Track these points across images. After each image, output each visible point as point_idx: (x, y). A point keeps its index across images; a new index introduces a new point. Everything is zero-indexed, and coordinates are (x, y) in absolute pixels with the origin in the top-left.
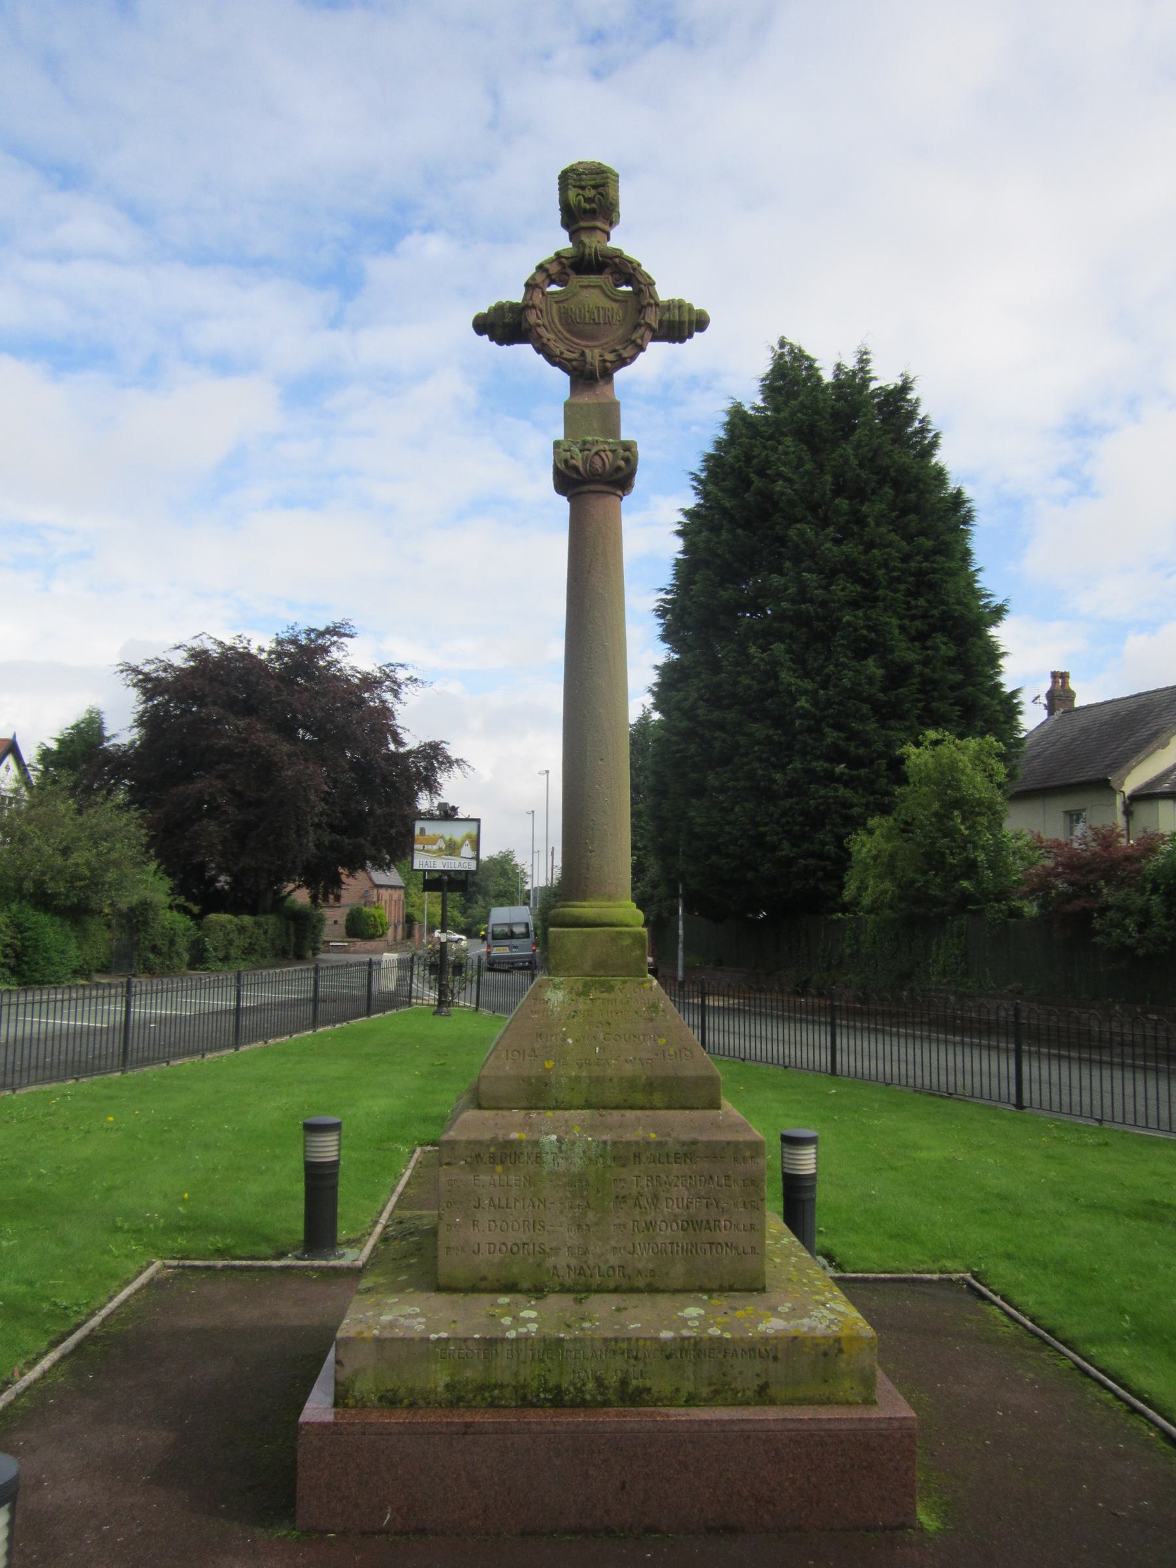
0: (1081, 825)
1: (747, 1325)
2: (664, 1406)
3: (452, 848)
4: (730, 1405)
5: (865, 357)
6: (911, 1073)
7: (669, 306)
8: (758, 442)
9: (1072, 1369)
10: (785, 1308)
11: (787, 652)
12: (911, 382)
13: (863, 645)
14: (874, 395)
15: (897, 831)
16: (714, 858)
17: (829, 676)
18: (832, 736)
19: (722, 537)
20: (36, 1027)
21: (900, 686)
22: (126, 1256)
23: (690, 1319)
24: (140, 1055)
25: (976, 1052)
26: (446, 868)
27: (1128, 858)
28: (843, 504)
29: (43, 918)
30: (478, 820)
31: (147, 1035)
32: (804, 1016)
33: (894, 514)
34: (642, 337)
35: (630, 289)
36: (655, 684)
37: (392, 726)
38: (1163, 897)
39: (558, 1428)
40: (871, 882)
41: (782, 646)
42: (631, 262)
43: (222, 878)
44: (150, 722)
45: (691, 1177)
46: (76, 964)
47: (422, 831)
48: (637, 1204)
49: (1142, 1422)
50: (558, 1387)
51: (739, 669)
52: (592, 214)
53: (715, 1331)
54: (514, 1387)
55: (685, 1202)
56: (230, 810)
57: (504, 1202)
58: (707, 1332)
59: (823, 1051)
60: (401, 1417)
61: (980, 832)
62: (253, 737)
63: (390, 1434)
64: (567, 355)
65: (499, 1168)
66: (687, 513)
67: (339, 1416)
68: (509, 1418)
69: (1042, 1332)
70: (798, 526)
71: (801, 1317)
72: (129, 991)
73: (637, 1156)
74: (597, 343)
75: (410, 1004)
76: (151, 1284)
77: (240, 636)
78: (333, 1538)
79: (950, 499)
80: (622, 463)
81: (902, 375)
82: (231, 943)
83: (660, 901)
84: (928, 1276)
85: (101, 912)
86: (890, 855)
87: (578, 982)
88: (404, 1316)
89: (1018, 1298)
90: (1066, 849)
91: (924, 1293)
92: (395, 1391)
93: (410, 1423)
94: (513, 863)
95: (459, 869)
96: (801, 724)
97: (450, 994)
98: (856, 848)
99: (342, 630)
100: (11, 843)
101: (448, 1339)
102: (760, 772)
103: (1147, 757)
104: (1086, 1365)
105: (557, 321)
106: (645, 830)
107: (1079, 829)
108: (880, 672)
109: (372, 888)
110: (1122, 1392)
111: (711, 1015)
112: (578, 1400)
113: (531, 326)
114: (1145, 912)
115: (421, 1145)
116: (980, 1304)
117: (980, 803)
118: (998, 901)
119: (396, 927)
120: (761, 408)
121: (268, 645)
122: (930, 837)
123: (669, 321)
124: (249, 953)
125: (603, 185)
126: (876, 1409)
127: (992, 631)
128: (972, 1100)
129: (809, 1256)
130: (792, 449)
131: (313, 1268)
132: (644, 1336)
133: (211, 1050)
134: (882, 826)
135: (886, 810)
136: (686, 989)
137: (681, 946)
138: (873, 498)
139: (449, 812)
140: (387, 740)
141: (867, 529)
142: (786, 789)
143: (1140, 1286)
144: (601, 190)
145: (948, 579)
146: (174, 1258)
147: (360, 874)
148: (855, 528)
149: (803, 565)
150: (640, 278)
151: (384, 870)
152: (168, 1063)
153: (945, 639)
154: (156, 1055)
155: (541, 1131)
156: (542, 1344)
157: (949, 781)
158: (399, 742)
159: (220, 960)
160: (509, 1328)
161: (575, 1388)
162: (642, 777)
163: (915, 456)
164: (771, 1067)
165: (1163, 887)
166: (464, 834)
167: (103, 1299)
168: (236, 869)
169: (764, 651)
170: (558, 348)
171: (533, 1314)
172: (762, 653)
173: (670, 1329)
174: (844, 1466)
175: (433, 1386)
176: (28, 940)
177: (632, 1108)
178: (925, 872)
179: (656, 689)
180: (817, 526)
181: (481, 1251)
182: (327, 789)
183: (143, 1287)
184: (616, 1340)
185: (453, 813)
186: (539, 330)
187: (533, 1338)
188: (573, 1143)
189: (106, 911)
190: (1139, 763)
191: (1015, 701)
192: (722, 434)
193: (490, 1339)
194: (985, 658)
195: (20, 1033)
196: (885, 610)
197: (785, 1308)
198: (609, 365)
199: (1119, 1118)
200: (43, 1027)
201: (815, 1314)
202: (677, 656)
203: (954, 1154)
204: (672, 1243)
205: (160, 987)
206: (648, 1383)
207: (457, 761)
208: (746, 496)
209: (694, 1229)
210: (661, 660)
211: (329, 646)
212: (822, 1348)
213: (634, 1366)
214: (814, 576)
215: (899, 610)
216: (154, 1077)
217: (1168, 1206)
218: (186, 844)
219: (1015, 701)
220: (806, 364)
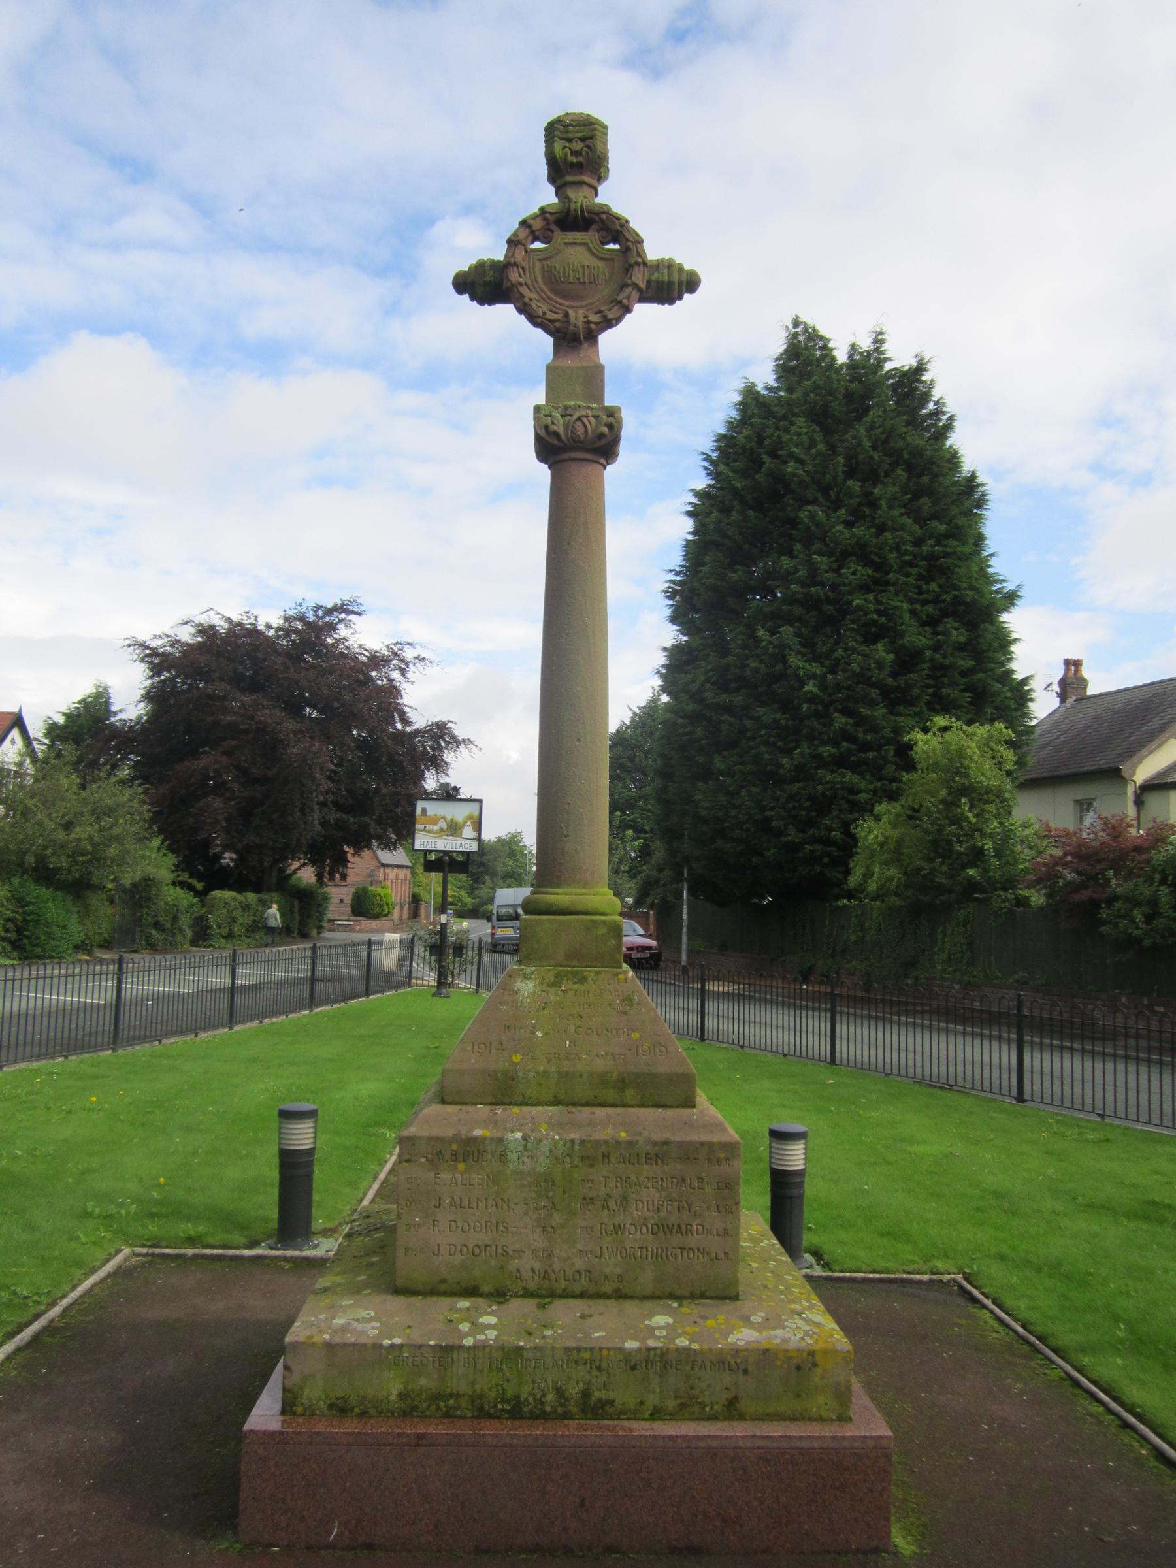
0: (1092, 814)
1: (717, 1336)
2: (628, 1419)
3: (454, 829)
4: (698, 1419)
5: (880, 337)
6: (911, 1063)
7: (658, 265)
9: (1062, 1379)
10: (757, 1318)
11: (797, 635)
12: (926, 363)
13: (873, 629)
14: (889, 375)
16: (719, 843)
17: (838, 660)
18: (840, 721)
19: (733, 518)
20: (32, 1002)
22: (94, 1243)
24: (131, 1033)
25: (977, 1042)
26: (447, 849)
27: (1137, 849)
28: (855, 485)
29: (45, 892)
30: (480, 801)
32: (810, 1004)
34: (628, 298)
35: (617, 247)
36: (663, 666)
37: (399, 704)
38: (1172, 889)
40: (877, 869)
41: (791, 629)
42: (618, 219)
44: (154, 696)
45: (662, 1179)
46: (78, 939)
47: (424, 810)
48: (605, 1206)
49: (1134, 1438)
50: (517, 1397)
52: (579, 167)
53: (682, 1342)
54: (471, 1396)
56: (236, 787)
58: (674, 1343)
60: (350, 1426)
63: (338, 1444)
64: (550, 316)
65: (461, 1166)
66: (697, 494)
67: (285, 1425)
68: (464, 1430)
69: (1032, 1339)
70: (809, 508)
71: (774, 1328)
72: (120, 969)
73: (606, 1156)
74: (583, 303)
75: (409, 985)
76: (117, 1273)
77: (248, 613)
78: (277, 1552)
80: (605, 430)
81: (916, 356)
82: (234, 920)
83: (665, 885)
84: (918, 1277)
85: (104, 887)
86: (897, 842)
87: (549, 972)
88: (357, 1320)
89: (1009, 1303)
90: (1075, 839)
93: (359, 1433)
95: (461, 849)
96: (808, 708)
98: (863, 834)
99: (350, 608)
100: (13, 817)
101: (402, 1346)
102: (767, 756)
103: (1159, 746)
104: (1077, 1375)
105: (539, 279)
107: (1090, 819)
109: (379, 867)
110: (1114, 1405)
111: (711, 1000)
112: (538, 1411)
113: (512, 285)
114: (1153, 903)
116: (973, 1309)
117: (988, 790)
118: (1005, 890)
119: (402, 906)
121: (276, 621)
122: (937, 824)
123: (658, 282)
124: (253, 931)
125: (591, 138)
127: (1004, 617)
128: (973, 1092)
129: (789, 1260)
131: (285, 1259)
132: (609, 1345)
133: (205, 1029)
135: (892, 796)
137: (685, 930)
138: (886, 481)
139: (451, 792)
141: (879, 512)
142: (793, 773)
143: (1136, 1291)
144: (588, 142)
146: (144, 1246)
147: (366, 853)
148: (867, 511)
149: (814, 548)
151: (390, 849)
152: (160, 1042)
153: (956, 625)
154: (148, 1034)
155: (505, 1129)
156: (500, 1353)
157: (957, 768)
158: (406, 721)
159: (224, 937)
160: (466, 1335)
162: (650, 760)
163: (929, 439)
164: (770, 1054)
165: (1170, 878)
167: (67, 1288)
168: (240, 846)
170: (541, 308)
171: (493, 1320)
172: (771, 636)
173: (635, 1339)
175: (385, 1394)
176: (29, 915)
177: (602, 1105)
178: (931, 860)
179: (664, 671)
180: (828, 507)
181: (441, 1253)
182: (332, 767)
183: (109, 1275)
184: (578, 1349)
185: (455, 793)
187: (491, 1346)
189: (110, 886)
190: (1151, 752)
191: (1026, 688)
193: (447, 1346)
194: (996, 645)
195: (16, 1008)
196: (897, 594)
197: (757, 1318)
198: (593, 326)
199: (1121, 1113)
200: (39, 1002)
201: (789, 1325)
202: (685, 638)
203: (950, 1149)
204: (641, 1248)
206: (611, 1395)
207: (464, 741)
208: (757, 477)
209: (665, 1233)
210: (669, 642)
211: (337, 624)
212: (795, 1361)
213: (597, 1376)
214: (825, 559)
215: (910, 594)
216: (144, 1056)
217: (1169, 1207)
218: (191, 820)
219: (1026, 688)
220: (821, 343)
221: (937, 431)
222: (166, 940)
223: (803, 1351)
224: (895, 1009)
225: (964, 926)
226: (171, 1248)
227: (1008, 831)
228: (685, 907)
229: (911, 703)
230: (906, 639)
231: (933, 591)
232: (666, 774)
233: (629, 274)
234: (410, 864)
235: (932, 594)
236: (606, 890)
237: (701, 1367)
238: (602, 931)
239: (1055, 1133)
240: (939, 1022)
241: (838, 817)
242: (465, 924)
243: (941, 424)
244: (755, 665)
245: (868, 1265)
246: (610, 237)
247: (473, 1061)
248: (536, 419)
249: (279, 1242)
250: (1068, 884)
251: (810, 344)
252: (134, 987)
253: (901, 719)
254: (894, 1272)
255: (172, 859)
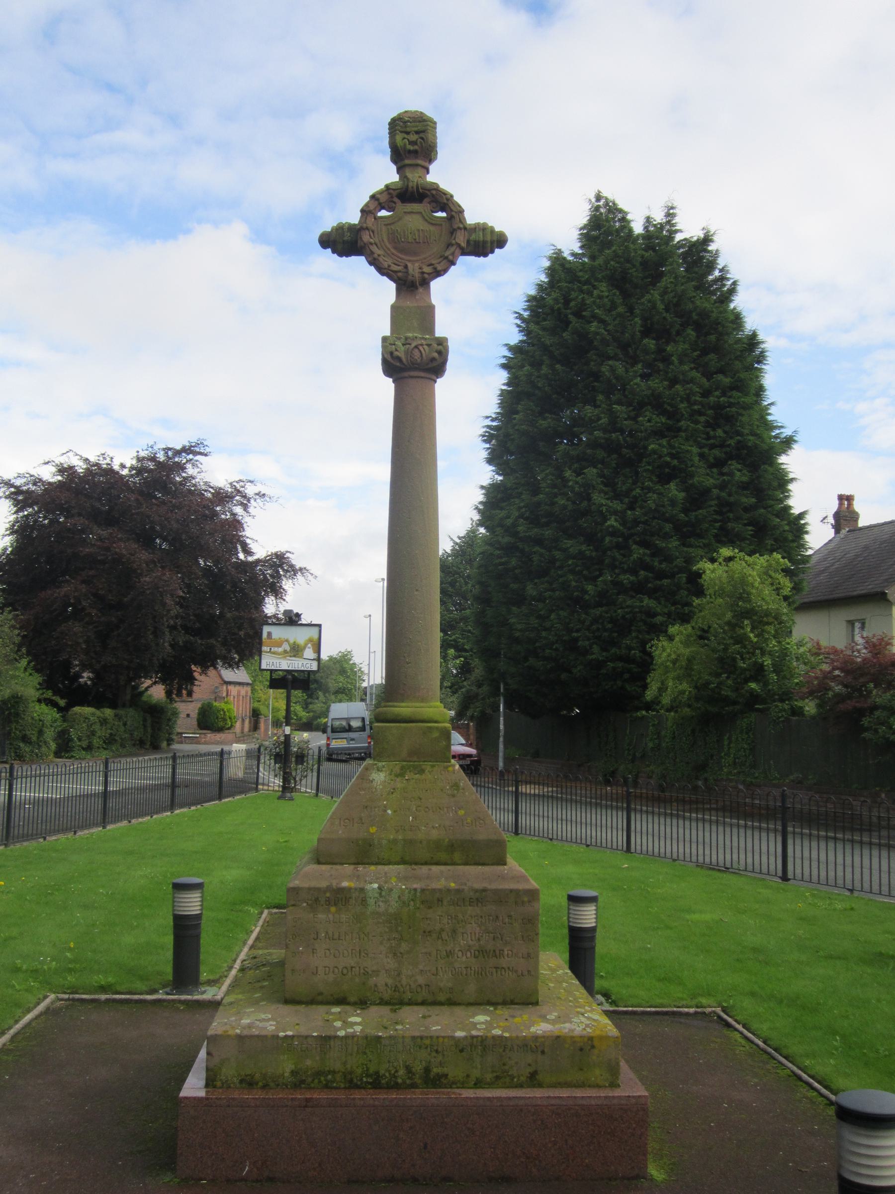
1: (522, 1028)
2: (458, 1088)
3: (296, 651)
4: (508, 1087)
5: (671, 211)
7: (475, 228)
8: (576, 287)
9: (789, 1076)
12: (712, 235)
13: (667, 470)
14: (680, 244)
15: (695, 637)
16: (532, 661)
17: (636, 499)
18: (638, 552)
19: (542, 372)
21: (700, 508)
22: (27, 990)
23: (479, 1023)
26: (290, 668)
28: (650, 343)
30: (319, 626)
31: (22, 815)
33: (696, 354)
34: (453, 254)
35: (444, 215)
36: (481, 503)
37: (242, 536)
39: (376, 1103)
41: (595, 471)
43: (85, 675)
45: (481, 917)
47: (269, 634)
50: (377, 1073)
51: (556, 490)
53: (497, 1032)
54: (343, 1073)
55: (477, 936)
56: (94, 612)
57: (336, 936)
59: (620, 833)
60: (258, 1094)
61: (767, 639)
62: (114, 545)
65: (333, 909)
66: (511, 348)
68: (341, 1096)
69: (770, 1050)
70: (610, 362)
71: (564, 1022)
73: (440, 900)
74: (418, 258)
75: (257, 790)
76: (47, 1011)
77: (104, 454)
78: (204, 1183)
79: (745, 341)
80: (436, 355)
81: (703, 229)
82: (93, 733)
83: (483, 699)
84: (686, 1010)
87: (397, 766)
88: (259, 1020)
89: (755, 1026)
91: (681, 1023)
92: (252, 1076)
94: (351, 662)
95: (302, 669)
97: (292, 781)
99: (197, 449)
101: (293, 1037)
102: (574, 584)
106: (472, 633)
108: (682, 495)
109: (222, 685)
110: (824, 1091)
113: (365, 244)
115: (268, 908)
116: (726, 1031)
117: (767, 613)
118: (782, 701)
119: (243, 721)
120: (579, 254)
121: (130, 462)
122: (723, 643)
123: (475, 241)
124: (110, 743)
125: (424, 132)
126: (619, 1090)
130: (607, 294)
131: (180, 1001)
132: (443, 1035)
133: (83, 827)
134: (681, 633)
135: (685, 619)
136: (506, 778)
137: (501, 739)
139: (294, 618)
140: (237, 549)
144: (422, 135)
145: (744, 412)
146: (65, 993)
147: (211, 672)
148: (661, 366)
150: (451, 205)
151: (233, 669)
152: (45, 839)
153: (739, 466)
154: (57, 828)
155: (366, 881)
156: (365, 1041)
157: (741, 594)
158: (248, 552)
159: (84, 749)
160: (340, 1029)
161: (390, 1074)
162: (470, 585)
163: (715, 302)
166: (307, 638)
167: (11, 1022)
168: (98, 667)
169: (578, 474)
170: (386, 262)
171: (358, 1020)
172: (577, 477)
173: (462, 1030)
174: (594, 1132)
175: (281, 1072)
178: (718, 675)
179: (481, 507)
182: (181, 594)
184: (421, 1038)
185: (297, 619)
186: (371, 247)
187: (358, 1036)
188: (391, 890)
191: (802, 522)
192: (544, 278)
194: (775, 484)
196: (687, 439)
197: (552, 1016)
198: (426, 276)
201: (575, 1020)
202: (500, 478)
204: (466, 968)
205: (38, 772)
206: (445, 1070)
207: (301, 569)
208: (564, 335)
210: (486, 482)
211: (184, 464)
212: (579, 1045)
214: (624, 408)
215: (699, 439)
219: (802, 522)
220: (620, 216)
221: (722, 295)
222: (33, 752)
223: (584, 1037)
224: (687, 807)
225: (747, 733)
226: (87, 994)
227: (785, 649)
228: (502, 718)
229: (700, 536)
230: (696, 479)
231: (720, 437)
232: (484, 600)
233: (453, 237)
234: (250, 682)
235: (718, 439)
236: (438, 704)
237: (510, 1050)
238: (436, 734)
239: (810, 904)
240: (724, 818)
241: (637, 637)
242: (306, 735)
243: (726, 289)
244: (563, 502)
245: (648, 1002)
246: (438, 208)
247: (340, 832)
248: (383, 347)
249: (175, 989)
250: (837, 695)
251: (611, 216)
252: (23, 793)
253: (691, 550)
254: (667, 1007)
255: (37, 679)
